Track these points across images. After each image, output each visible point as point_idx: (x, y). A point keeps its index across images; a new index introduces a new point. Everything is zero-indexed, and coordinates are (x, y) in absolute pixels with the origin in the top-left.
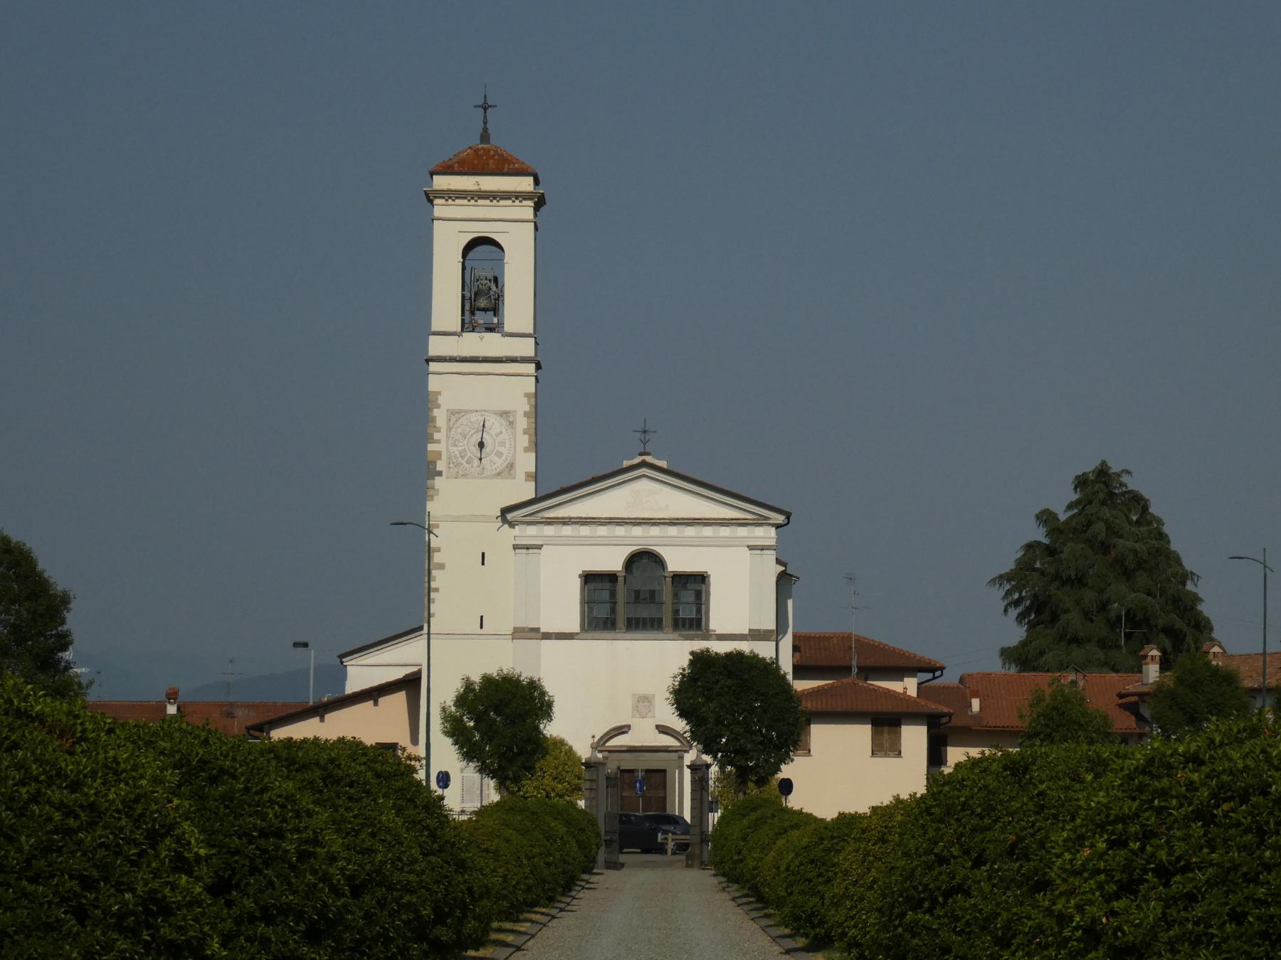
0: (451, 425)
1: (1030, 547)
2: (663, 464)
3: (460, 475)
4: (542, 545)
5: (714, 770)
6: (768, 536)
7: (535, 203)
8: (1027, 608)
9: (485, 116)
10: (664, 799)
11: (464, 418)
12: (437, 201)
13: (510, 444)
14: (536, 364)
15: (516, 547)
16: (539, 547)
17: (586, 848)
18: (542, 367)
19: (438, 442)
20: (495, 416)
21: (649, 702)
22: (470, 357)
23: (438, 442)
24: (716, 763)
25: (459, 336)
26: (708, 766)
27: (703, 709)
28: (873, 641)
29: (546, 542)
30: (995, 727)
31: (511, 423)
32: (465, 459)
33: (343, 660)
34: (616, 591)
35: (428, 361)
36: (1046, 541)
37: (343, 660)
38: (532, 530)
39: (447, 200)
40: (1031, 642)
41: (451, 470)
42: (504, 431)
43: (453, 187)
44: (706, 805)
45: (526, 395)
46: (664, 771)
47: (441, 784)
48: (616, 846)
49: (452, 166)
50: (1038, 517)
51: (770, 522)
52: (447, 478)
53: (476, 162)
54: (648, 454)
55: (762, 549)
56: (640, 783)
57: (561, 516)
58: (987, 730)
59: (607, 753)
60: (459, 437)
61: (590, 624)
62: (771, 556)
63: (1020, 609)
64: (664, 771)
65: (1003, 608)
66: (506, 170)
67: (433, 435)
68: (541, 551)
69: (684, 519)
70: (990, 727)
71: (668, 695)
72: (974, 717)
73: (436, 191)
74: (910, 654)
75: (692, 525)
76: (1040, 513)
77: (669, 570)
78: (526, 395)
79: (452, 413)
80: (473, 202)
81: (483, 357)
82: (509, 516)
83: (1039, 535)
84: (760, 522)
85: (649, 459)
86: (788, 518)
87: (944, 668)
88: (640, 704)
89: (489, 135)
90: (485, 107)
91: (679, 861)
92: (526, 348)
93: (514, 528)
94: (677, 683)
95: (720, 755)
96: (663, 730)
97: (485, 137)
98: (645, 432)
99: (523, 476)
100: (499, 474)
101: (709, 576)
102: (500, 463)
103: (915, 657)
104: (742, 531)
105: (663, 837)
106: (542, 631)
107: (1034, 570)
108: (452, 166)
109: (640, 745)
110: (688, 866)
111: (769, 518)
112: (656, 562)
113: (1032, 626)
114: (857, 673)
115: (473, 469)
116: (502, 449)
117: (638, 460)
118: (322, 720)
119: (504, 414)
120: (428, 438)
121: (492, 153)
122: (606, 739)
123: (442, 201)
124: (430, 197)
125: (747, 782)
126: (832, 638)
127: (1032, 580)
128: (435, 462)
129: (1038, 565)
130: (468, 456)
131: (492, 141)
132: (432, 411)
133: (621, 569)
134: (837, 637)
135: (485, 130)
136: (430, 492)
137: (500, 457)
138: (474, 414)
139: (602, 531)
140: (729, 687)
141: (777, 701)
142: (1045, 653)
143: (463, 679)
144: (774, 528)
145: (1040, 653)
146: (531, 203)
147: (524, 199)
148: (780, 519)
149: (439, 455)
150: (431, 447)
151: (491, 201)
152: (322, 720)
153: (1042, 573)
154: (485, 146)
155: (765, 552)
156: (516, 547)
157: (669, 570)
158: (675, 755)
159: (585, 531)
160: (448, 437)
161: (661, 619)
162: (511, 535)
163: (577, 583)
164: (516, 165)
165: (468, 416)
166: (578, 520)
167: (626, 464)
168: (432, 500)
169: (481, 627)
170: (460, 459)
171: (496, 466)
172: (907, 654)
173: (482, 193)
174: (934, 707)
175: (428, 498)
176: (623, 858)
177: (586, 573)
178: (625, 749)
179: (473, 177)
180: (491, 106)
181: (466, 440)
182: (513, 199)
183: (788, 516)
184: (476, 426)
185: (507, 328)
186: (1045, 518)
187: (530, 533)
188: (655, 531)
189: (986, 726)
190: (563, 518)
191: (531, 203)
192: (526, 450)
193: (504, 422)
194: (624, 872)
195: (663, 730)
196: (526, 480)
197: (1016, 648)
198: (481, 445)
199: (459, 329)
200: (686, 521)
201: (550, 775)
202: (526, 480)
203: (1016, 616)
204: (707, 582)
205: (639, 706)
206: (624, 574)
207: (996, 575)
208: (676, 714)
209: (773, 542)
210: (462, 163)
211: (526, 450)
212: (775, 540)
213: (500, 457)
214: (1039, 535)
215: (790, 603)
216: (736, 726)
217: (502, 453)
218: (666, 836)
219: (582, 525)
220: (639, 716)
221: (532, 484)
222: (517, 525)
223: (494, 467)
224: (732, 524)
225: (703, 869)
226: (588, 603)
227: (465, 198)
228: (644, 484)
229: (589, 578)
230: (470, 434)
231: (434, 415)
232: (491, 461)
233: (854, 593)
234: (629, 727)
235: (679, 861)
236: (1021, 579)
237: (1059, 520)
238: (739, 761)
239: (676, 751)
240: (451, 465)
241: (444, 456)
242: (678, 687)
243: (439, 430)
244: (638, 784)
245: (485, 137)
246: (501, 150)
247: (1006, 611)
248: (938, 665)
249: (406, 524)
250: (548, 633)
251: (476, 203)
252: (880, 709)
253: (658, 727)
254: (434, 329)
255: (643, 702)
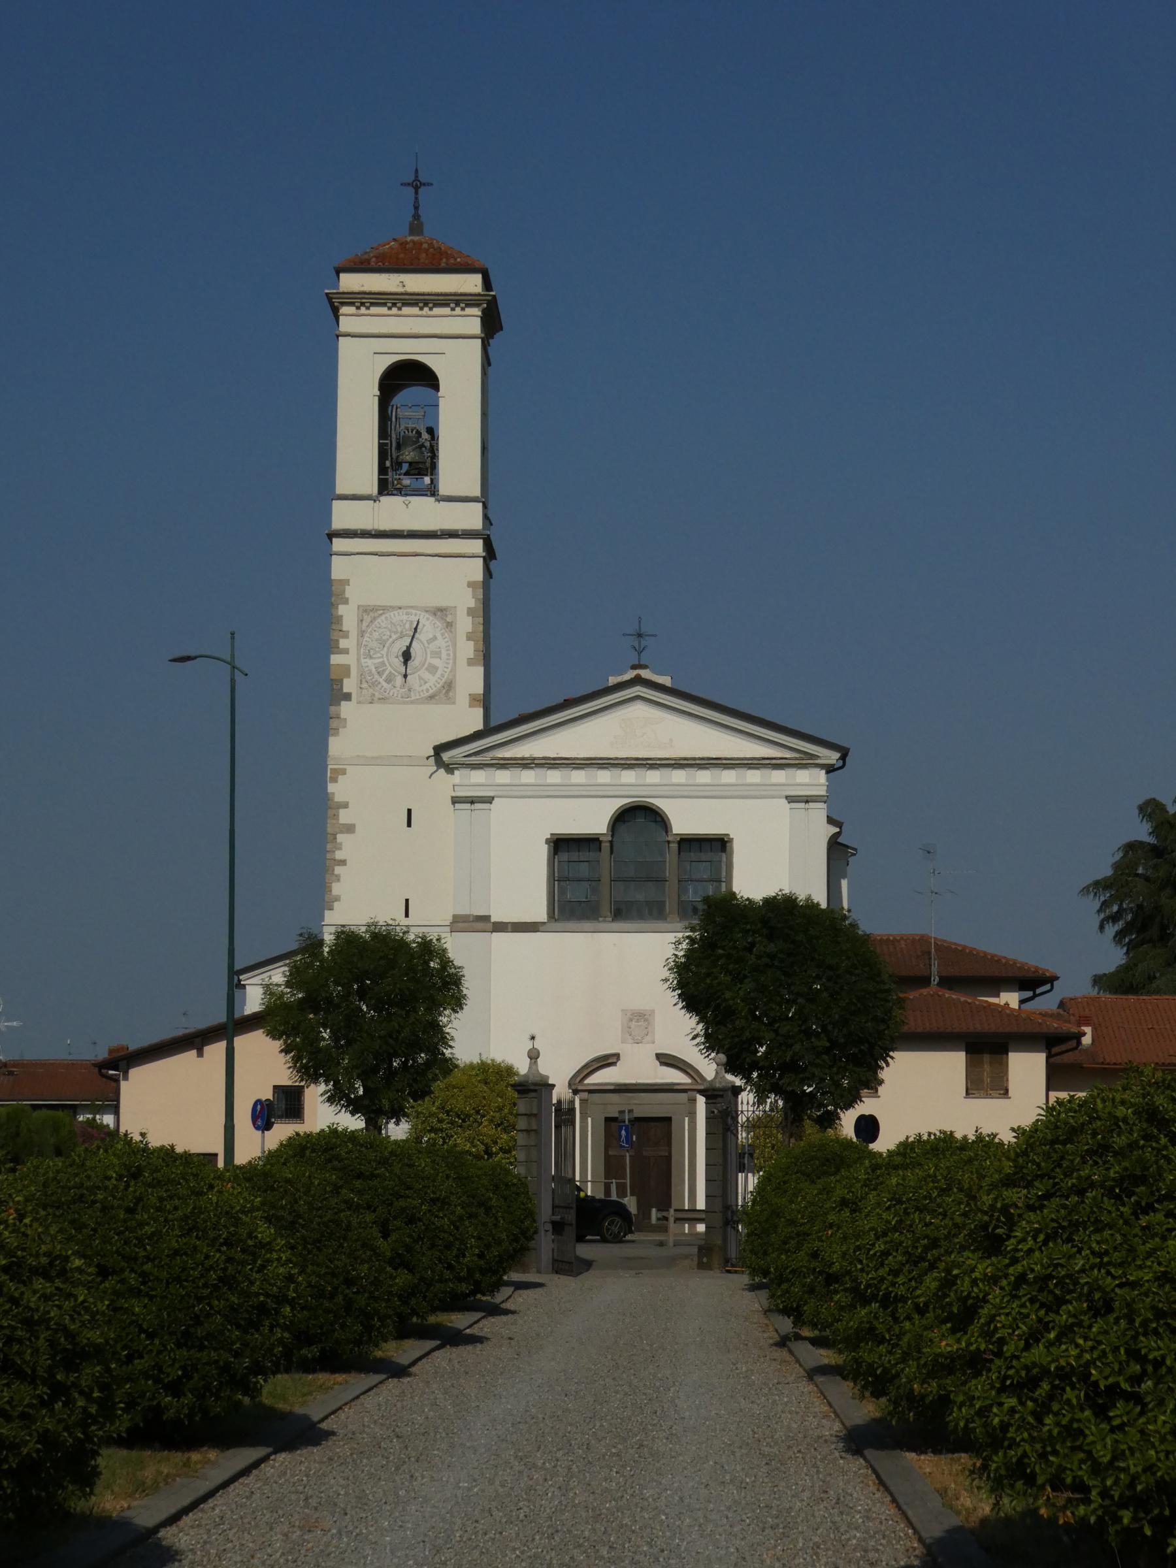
0: (364, 628)
1: (1131, 847)
2: (666, 680)
3: (376, 699)
4: (493, 798)
5: (747, 1099)
6: (815, 782)
7: (483, 311)
8: (1127, 923)
9: (416, 198)
10: (668, 1159)
11: (383, 617)
12: (344, 310)
13: (448, 655)
14: (484, 539)
15: (455, 801)
16: (489, 800)
17: (448, 1247)
18: (497, 555)
19: (346, 651)
20: (427, 615)
21: (646, 1020)
22: (391, 531)
23: (346, 651)
24: (749, 1088)
25: (375, 501)
26: (736, 1091)
27: (728, 995)
28: (955, 944)
29: (500, 793)
30: (1115, 1064)
31: (449, 625)
32: (384, 676)
33: (241, 977)
34: (711, 1270)
35: (331, 536)
36: (1151, 840)
37: (241, 977)
38: (478, 776)
39: (358, 308)
40: (1135, 965)
41: (364, 692)
42: (439, 636)
43: (366, 289)
44: (733, 1159)
45: (471, 584)
46: (669, 1119)
47: (259, 1123)
48: (570, 1233)
49: (368, 261)
50: (1141, 809)
51: (816, 762)
52: (359, 703)
53: (402, 256)
54: (644, 667)
55: (807, 802)
56: (627, 1131)
57: (519, 756)
58: (1105, 1068)
59: (586, 1094)
60: (375, 645)
61: (561, 911)
62: (819, 812)
63: (1120, 925)
64: (669, 1119)
65: (1097, 924)
66: (443, 265)
67: (337, 641)
68: (492, 806)
69: (694, 759)
70: (1109, 1064)
71: (666, 973)
72: (1087, 1051)
73: (344, 293)
74: (1008, 960)
75: (707, 768)
76: (1144, 804)
77: (674, 832)
78: (471, 584)
79: (365, 611)
80: (394, 311)
81: (409, 531)
82: (446, 756)
83: (1142, 832)
84: (805, 762)
85: (645, 674)
86: (843, 758)
87: (1057, 978)
88: (633, 1024)
89: (422, 224)
90: (417, 185)
91: (686, 1257)
92: (471, 517)
93: (453, 773)
94: (681, 953)
95: (755, 1075)
96: (666, 1060)
97: (416, 227)
98: (640, 635)
99: (467, 701)
100: (432, 697)
101: (731, 840)
102: (433, 682)
103: (1015, 963)
104: (778, 776)
105: (660, 1216)
106: (493, 920)
107: (1137, 875)
108: (368, 261)
109: (633, 1081)
110: (701, 1266)
111: (818, 757)
112: (656, 822)
113: (1131, 947)
114: (938, 984)
115: (395, 690)
116: (436, 662)
117: (630, 675)
118: (200, 1054)
119: (440, 612)
120: (333, 648)
121: (425, 246)
122: (585, 1073)
123: (351, 310)
124: (335, 304)
125: (803, 1120)
126: (898, 941)
127: (1135, 887)
128: (342, 680)
129: (1140, 871)
130: (387, 672)
131: (428, 232)
132: (337, 608)
133: (605, 831)
134: (905, 941)
135: (416, 216)
136: (334, 724)
137: (434, 674)
138: (396, 612)
139: (578, 777)
140: (772, 957)
141: (854, 979)
142: (1155, 978)
143: (301, 935)
144: (823, 772)
145: (1149, 977)
146: (477, 311)
147: (468, 305)
148: (833, 757)
149: (346, 670)
150: (335, 659)
151: (421, 309)
152: (200, 1054)
153: (1147, 879)
154: (416, 238)
155: (811, 805)
156: (455, 801)
157: (674, 832)
158: (683, 1097)
159: (554, 776)
160: (359, 645)
161: (663, 903)
162: (448, 784)
163: (542, 852)
164: (459, 260)
165: (387, 615)
166: (543, 761)
167: (613, 680)
168: (336, 734)
169: (407, 915)
170: (377, 676)
171: (427, 685)
172: (1004, 961)
173: (407, 297)
174: (1055, 1025)
175: (331, 732)
176: (584, 1251)
177: (555, 837)
178: (612, 1087)
179: (396, 275)
180: (424, 184)
181: (385, 649)
182: (452, 305)
183: (844, 754)
184: (399, 629)
185: (443, 490)
186: (1149, 810)
187: (476, 780)
188: (653, 776)
189: (1103, 1063)
190: (523, 759)
191: (477, 311)
192: (471, 662)
193: (438, 624)
194: (588, 1279)
195: (666, 1060)
196: (470, 706)
197: (1112, 975)
198: (407, 656)
199: (375, 491)
200: (698, 762)
201: (491, 1121)
202: (470, 706)
203: (1113, 934)
204: (728, 848)
205: (632, 1026)
206: (610, 839)
207: (1090, 881)
208: (680, 1005)
209: (822, 792)
210: (381, 257)
211: (471, 662)
212: (825, 788)
213: (434, 674)
214: (1142, 832)
215: (844, 884)
216: (785, 1023)
217: (437, 668)
218: (665, 1214)
219: (549, 768)
220: (631, 1041)
221: (479, 712)
222: (457, 768)
223: (424, 687)
224: (765, 766)
225: (729, 1272)
226: (558, 880)
227: (384, 304)
228: (639, 711)
229: (560, 845)
230: (391, 640)
231: (340, 613)
232: (420, 678)
233: (934, 873)
234: (617, 1056)
235: (686, 1257)
236: (1122, 886)
237: (1167, 812)
238: (789, 1084)
239: (685, 1091)
240: (364, 685)
241: (354, 672)
242: (683, 960)
243: (346, 635)
244: (623, 1132)
245: (416, 227)
246: (438, 242)
247: (1102, 928)
248: (1048, 974)
249: (195, 658)
250: (502, 923)
251: (400, 312)
252: (979, 1028)
253: (659, 1056)
254: (340, 489)
255: (638, 1021)
